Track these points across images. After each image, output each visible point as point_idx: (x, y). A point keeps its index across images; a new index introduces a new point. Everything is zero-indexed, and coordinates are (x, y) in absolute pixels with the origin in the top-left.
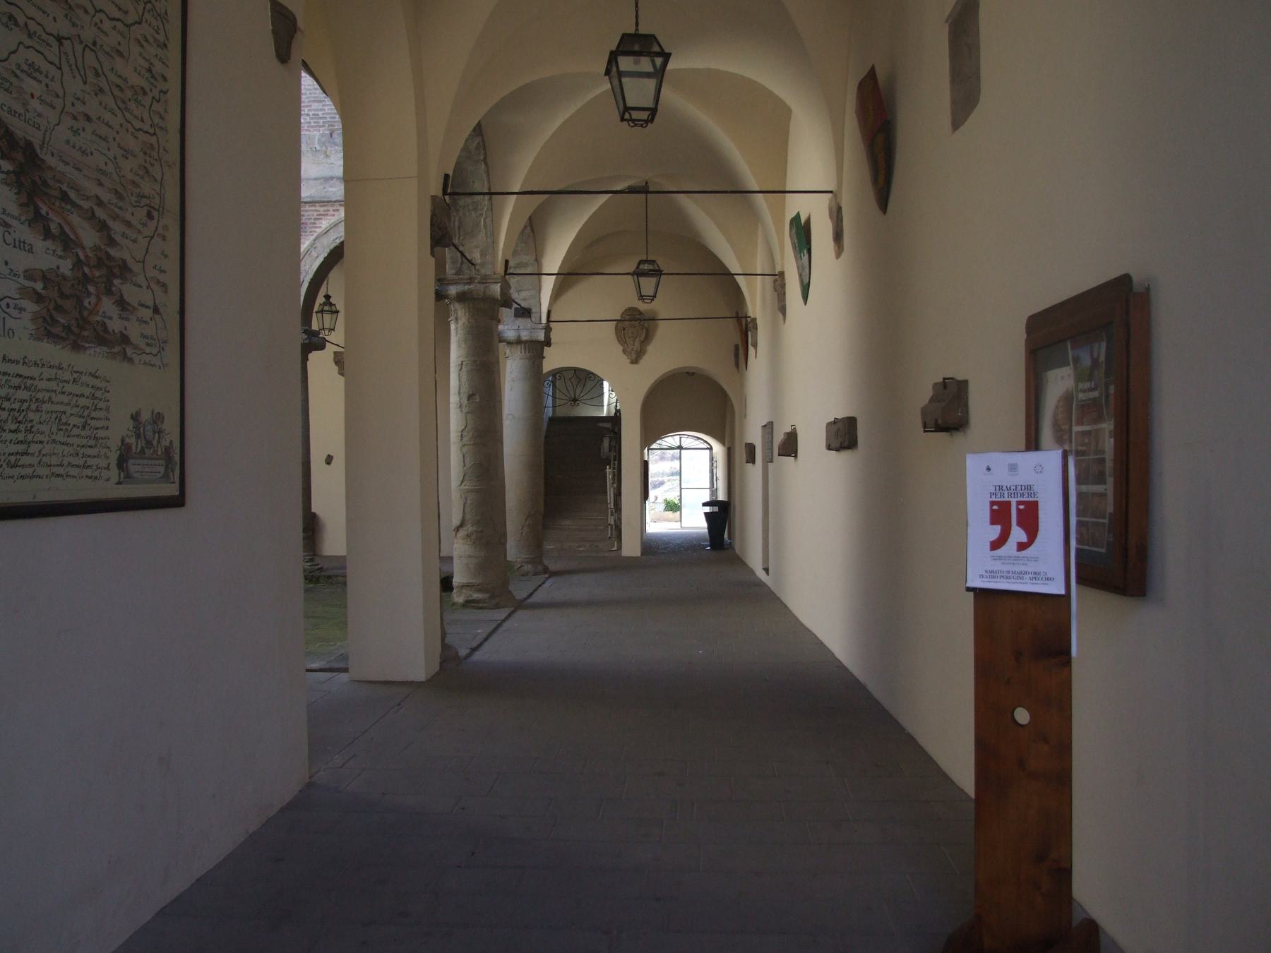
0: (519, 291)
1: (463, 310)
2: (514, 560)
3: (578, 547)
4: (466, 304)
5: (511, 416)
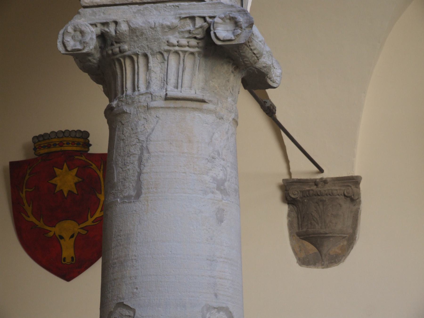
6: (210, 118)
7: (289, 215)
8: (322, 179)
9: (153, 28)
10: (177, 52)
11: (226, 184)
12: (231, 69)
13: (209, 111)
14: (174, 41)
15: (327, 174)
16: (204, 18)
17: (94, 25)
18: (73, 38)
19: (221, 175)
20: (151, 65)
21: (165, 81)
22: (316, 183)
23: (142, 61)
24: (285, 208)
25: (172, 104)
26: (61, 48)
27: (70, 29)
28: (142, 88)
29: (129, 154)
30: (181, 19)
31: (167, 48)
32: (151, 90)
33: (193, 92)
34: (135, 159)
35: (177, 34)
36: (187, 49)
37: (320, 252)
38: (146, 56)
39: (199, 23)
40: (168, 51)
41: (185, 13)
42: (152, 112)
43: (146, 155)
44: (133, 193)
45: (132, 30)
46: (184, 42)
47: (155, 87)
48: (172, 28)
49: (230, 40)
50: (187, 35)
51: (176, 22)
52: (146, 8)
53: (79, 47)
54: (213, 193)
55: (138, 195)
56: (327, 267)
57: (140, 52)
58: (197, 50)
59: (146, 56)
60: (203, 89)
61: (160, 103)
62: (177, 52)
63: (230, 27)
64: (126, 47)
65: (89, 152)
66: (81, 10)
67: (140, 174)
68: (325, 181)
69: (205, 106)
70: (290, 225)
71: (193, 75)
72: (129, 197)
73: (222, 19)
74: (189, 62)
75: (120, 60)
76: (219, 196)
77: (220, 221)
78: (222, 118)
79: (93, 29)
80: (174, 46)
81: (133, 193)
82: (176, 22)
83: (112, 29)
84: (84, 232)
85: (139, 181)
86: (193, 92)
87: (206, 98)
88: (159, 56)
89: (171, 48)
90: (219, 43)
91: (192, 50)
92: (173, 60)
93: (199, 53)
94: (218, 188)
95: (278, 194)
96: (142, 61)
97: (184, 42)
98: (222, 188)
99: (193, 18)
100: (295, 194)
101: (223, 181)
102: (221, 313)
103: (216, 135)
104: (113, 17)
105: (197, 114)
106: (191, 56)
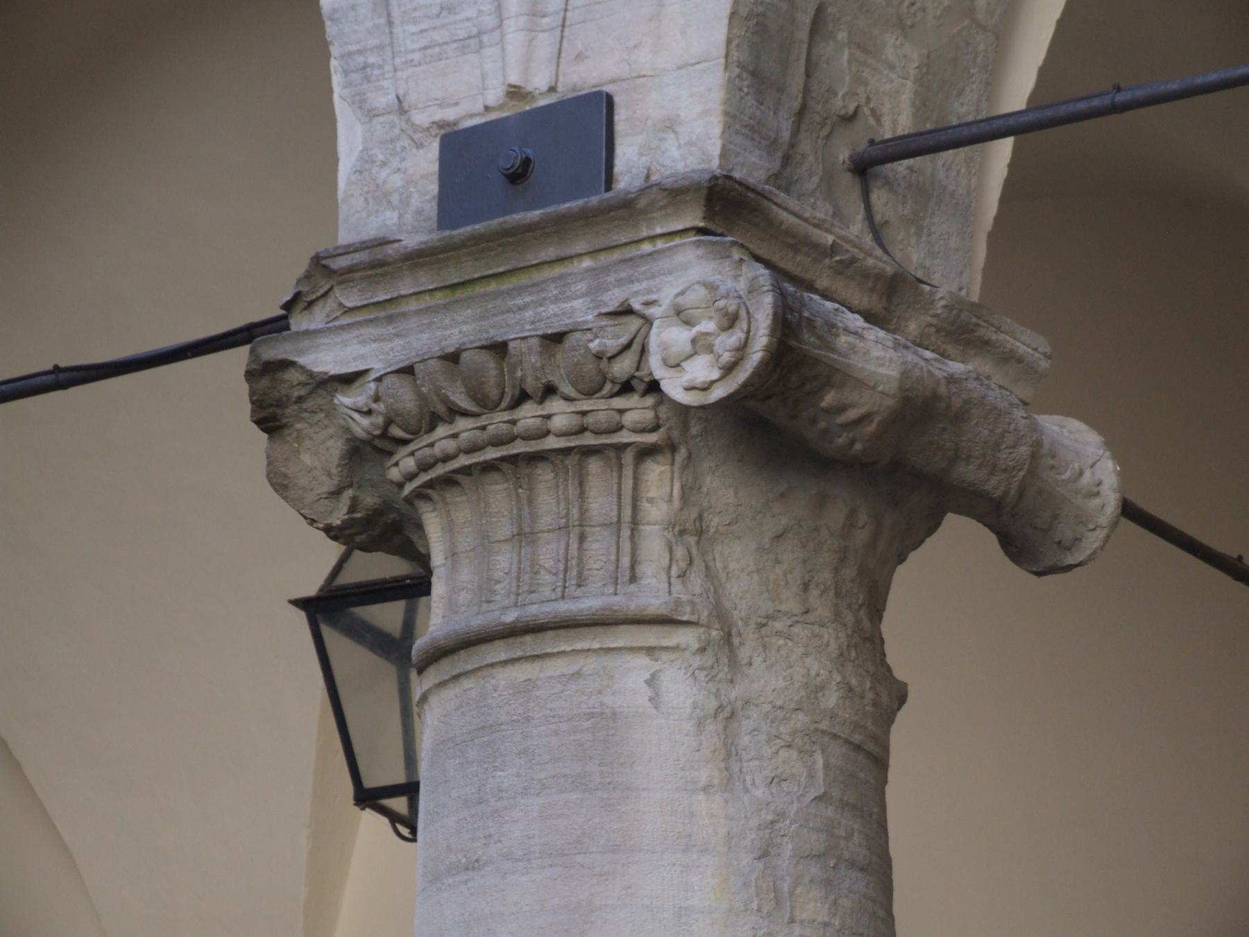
1: (790, 553)
4: (836, 515)
37: (1055, 542)
44: (789, 576)
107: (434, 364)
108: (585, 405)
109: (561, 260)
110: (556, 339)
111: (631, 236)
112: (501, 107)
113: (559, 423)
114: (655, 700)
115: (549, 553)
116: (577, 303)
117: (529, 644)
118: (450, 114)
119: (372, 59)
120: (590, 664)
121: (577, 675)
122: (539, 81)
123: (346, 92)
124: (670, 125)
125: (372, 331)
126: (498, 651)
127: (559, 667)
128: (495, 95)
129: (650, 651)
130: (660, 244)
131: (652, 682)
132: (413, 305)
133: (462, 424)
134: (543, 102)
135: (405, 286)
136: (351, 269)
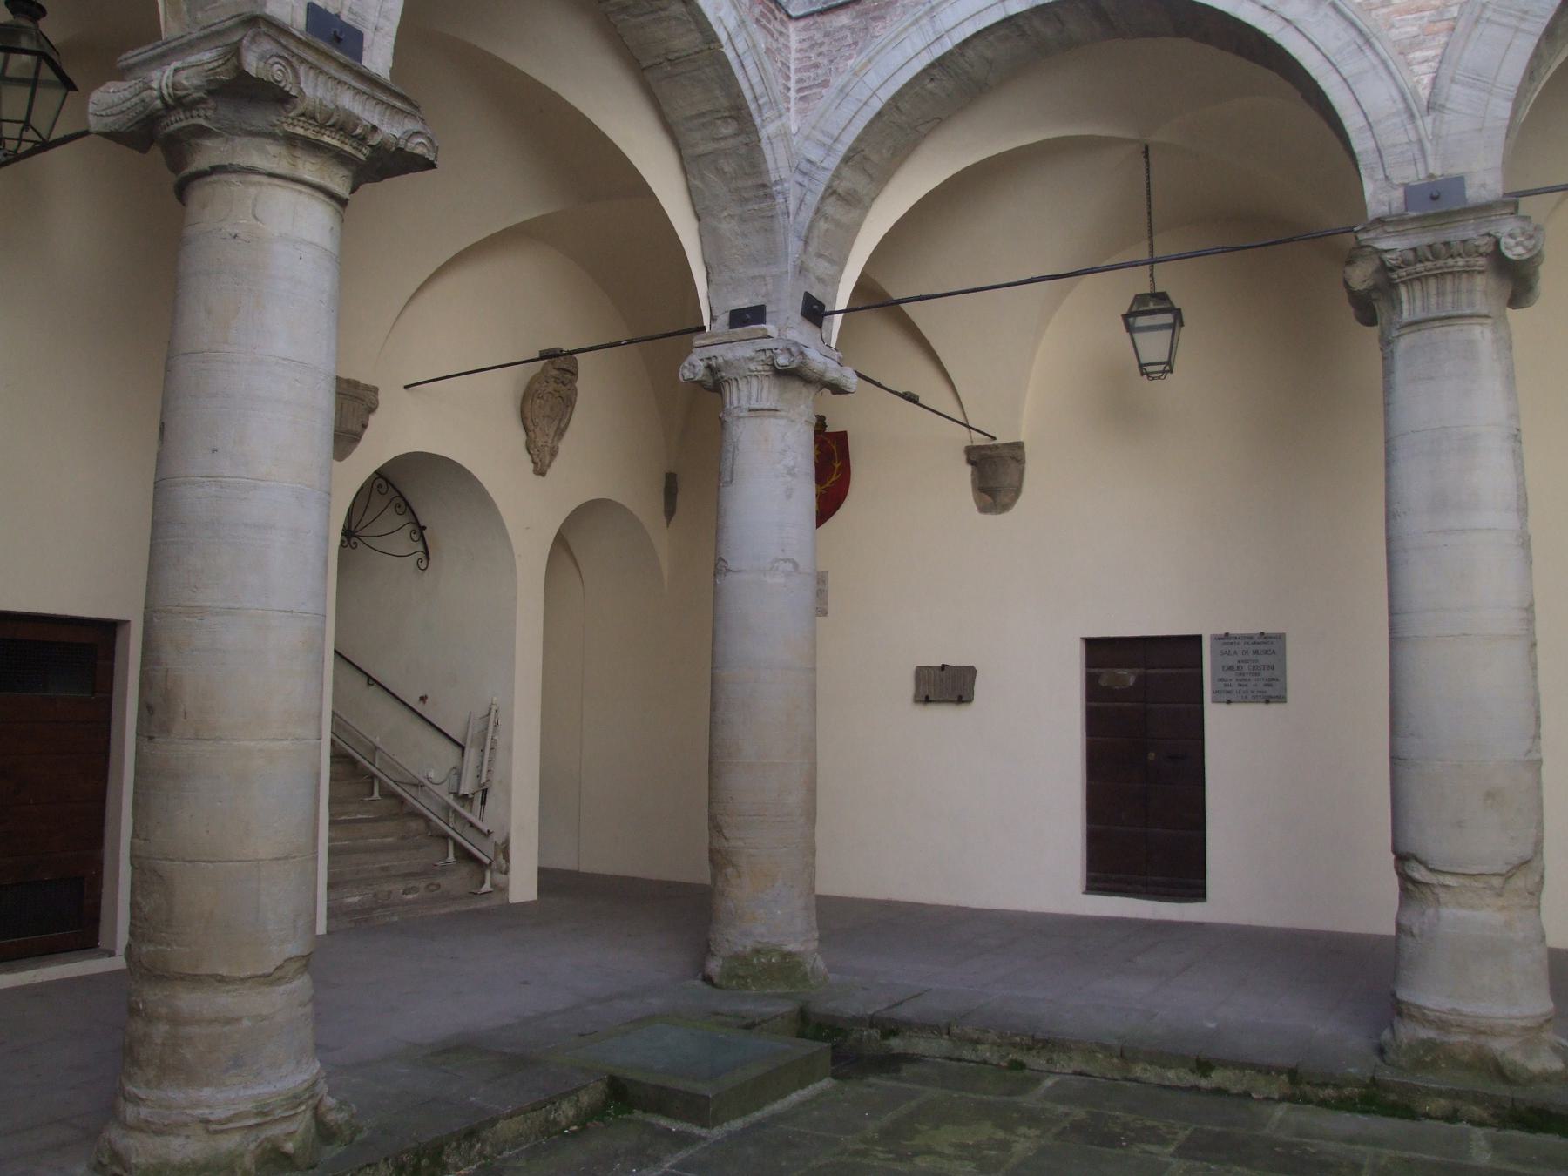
0: (820, 256)
2: (802, 948)
3: (405, 893)
5: (789, 566)
6: (783, 422)
7: (972, 474)
8: (994, 445)
9: (739, 360)
10: (756, 376)
11: (796, 469)
12: (802, 384)
13: (782, 417)
14: (753, 368)
15: (999, 441)
16: (771, 350)
17: (702, 360)
18: (689, 370)
19: (792, 463)
20: (740, 386)
21: (749, 398)
22: (990, 448)
23: (734, 383)
24: (969, 469)
25: (753, 414)
26: (681, 379)
27: (686, 364)
28: (736, 404)
29: (729, 451)
30: (757, 351)
31: (749, 373)
32: (740, 405)
33: (769, 404)
34: (730, 455)
35: (755, 363)
36: (763, 373)
37: (995, 502)
38: (736, 380)
39: (768, 354)
40: (750, 376)
41: (759, 347)
42: (742, 420)
43: (736, 452)
44: (729, 479)
45: (726, 362)
46: (760, 368)
47: (743, 403)
48: (751, 359)
49: (786, 366)
50: (762, 363)
51: (753, 354)
52: (734, 346)
53: (692, 377)
54: (784, 477)
55: (731, 481)
56: (1000, 513)
57: (733, 377)
58: (770, 373)
59: (736, 380)
60: (778, 400)
61: (745, 414)
62: (756, 376)
63: (787, 355)
64: (724, 374)
65: (827, 431)
66: (694, 350)
67: (733, 465)
68: (996, 447)
69: (778, 413)
70: (973, 482)
71: (769, 391)
72: (726, 482)
73: (782, 350)
74: (766, 383)
75: (1433, 256)
76: (789, 478)
77: (789, 497)
78: (793, 421)
79: (701, 363)
80: (753, 371)
81: (729, 479)
82: (753, 354)
83: (713, 362)
84: (824, 492)
85: (732, 473)
86: (769, 404)
87: (778, 408)
88: (745, 380)
89: (753, 374)
90: (780, 368)
91: (766, 373)
92: (754, 381)
93: (773, 375)
94: (789, 473)
95: (963, 458)
96: (734, 383)
97: (760, 368)
98: (792, 472)
99: (764, 350)
100: (974, 457)
101: (793, 468)
102: (788, 563)
103: (789, 434)
104: (712, 354)
105: (773, 420)
106: (767, 378)
107: (1425, 247)
108: (1467, 259)
109: (1463, 221)
110: (1464, 242)
111: (310, 38)
112: (1424, 180)
113: (1461, 264)
114: (1483, 337)
115: (1449, 298)
116: (1470, 232)
117: (1450, 322)
118: (1406, 181)
119: (1374, 165)
120: (1465, 327)
121: (1461, 330)
122: (1438, 173)
123: (798, 55)
124: (1483, 186)
125: (1397, 238)
126: (1437, 323)
127: (1456, 328)
128: (1422, 175)
129: (1481, 324)
130: (1498, 217)
131: (1482, 332)
132: (1411, 232)
133: (1459, 259)
134: (1440, 179)
135: (1409, 226)
136: (1391, 222)
